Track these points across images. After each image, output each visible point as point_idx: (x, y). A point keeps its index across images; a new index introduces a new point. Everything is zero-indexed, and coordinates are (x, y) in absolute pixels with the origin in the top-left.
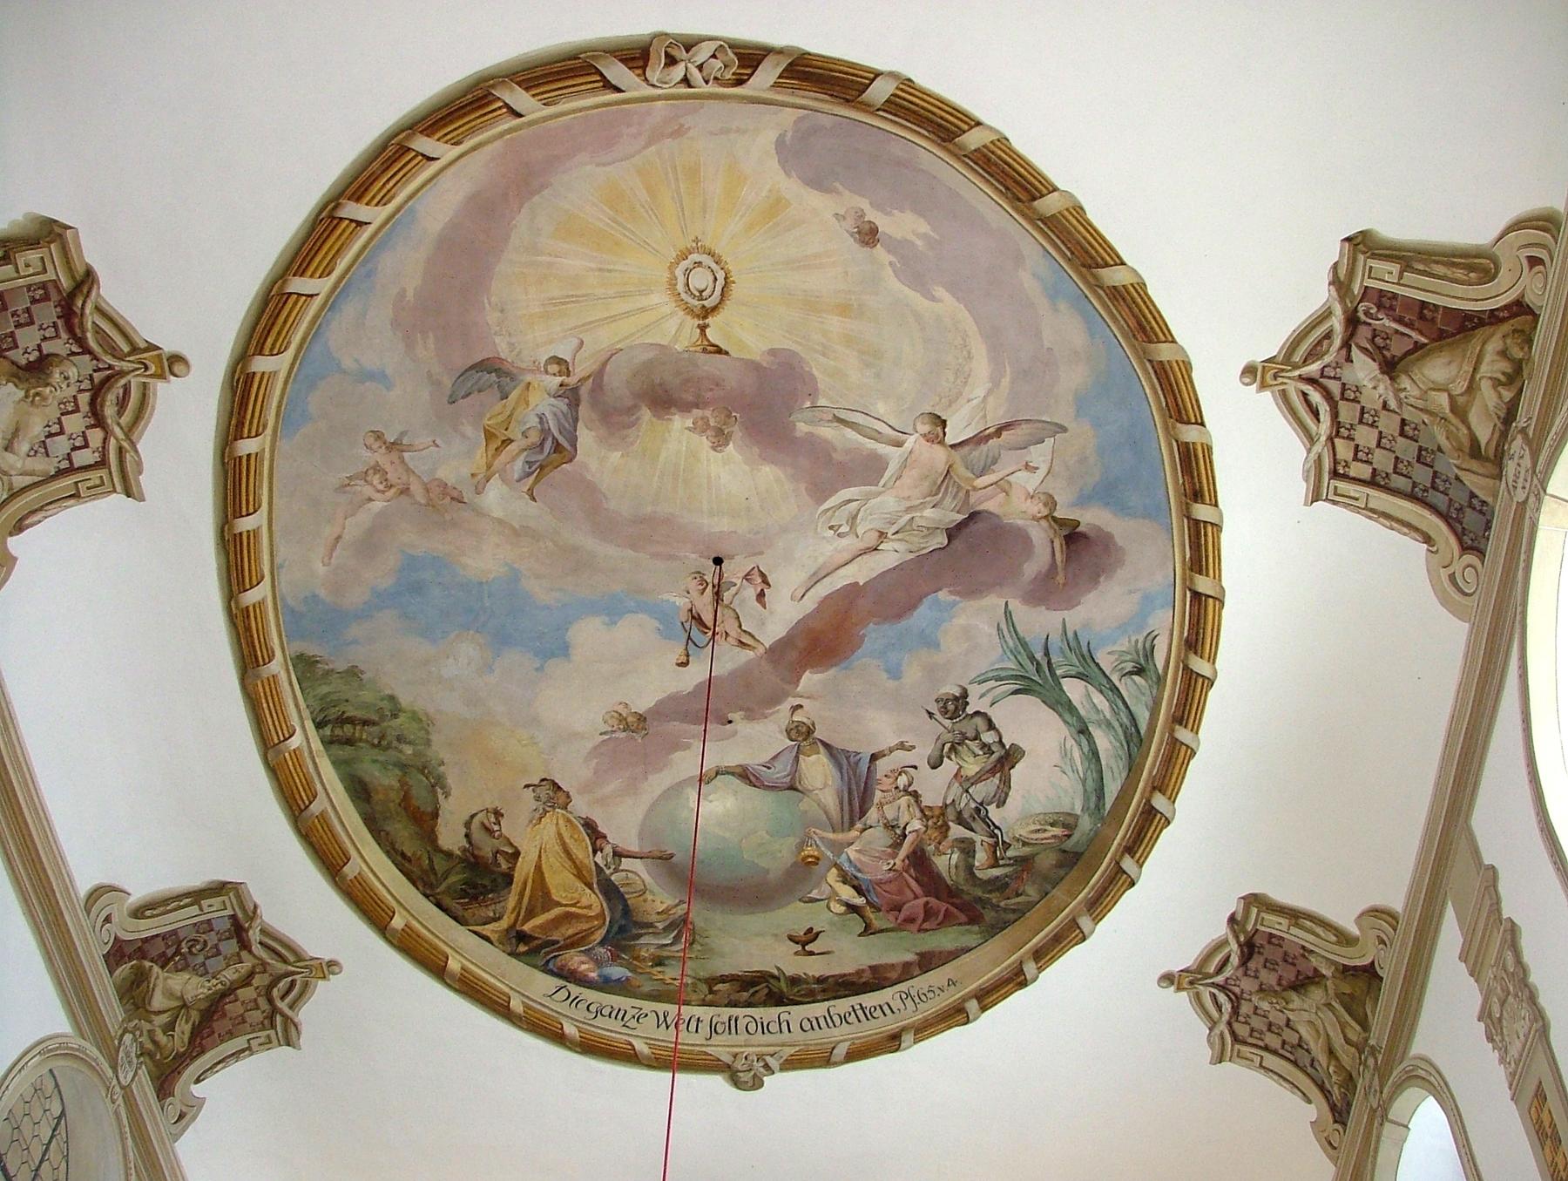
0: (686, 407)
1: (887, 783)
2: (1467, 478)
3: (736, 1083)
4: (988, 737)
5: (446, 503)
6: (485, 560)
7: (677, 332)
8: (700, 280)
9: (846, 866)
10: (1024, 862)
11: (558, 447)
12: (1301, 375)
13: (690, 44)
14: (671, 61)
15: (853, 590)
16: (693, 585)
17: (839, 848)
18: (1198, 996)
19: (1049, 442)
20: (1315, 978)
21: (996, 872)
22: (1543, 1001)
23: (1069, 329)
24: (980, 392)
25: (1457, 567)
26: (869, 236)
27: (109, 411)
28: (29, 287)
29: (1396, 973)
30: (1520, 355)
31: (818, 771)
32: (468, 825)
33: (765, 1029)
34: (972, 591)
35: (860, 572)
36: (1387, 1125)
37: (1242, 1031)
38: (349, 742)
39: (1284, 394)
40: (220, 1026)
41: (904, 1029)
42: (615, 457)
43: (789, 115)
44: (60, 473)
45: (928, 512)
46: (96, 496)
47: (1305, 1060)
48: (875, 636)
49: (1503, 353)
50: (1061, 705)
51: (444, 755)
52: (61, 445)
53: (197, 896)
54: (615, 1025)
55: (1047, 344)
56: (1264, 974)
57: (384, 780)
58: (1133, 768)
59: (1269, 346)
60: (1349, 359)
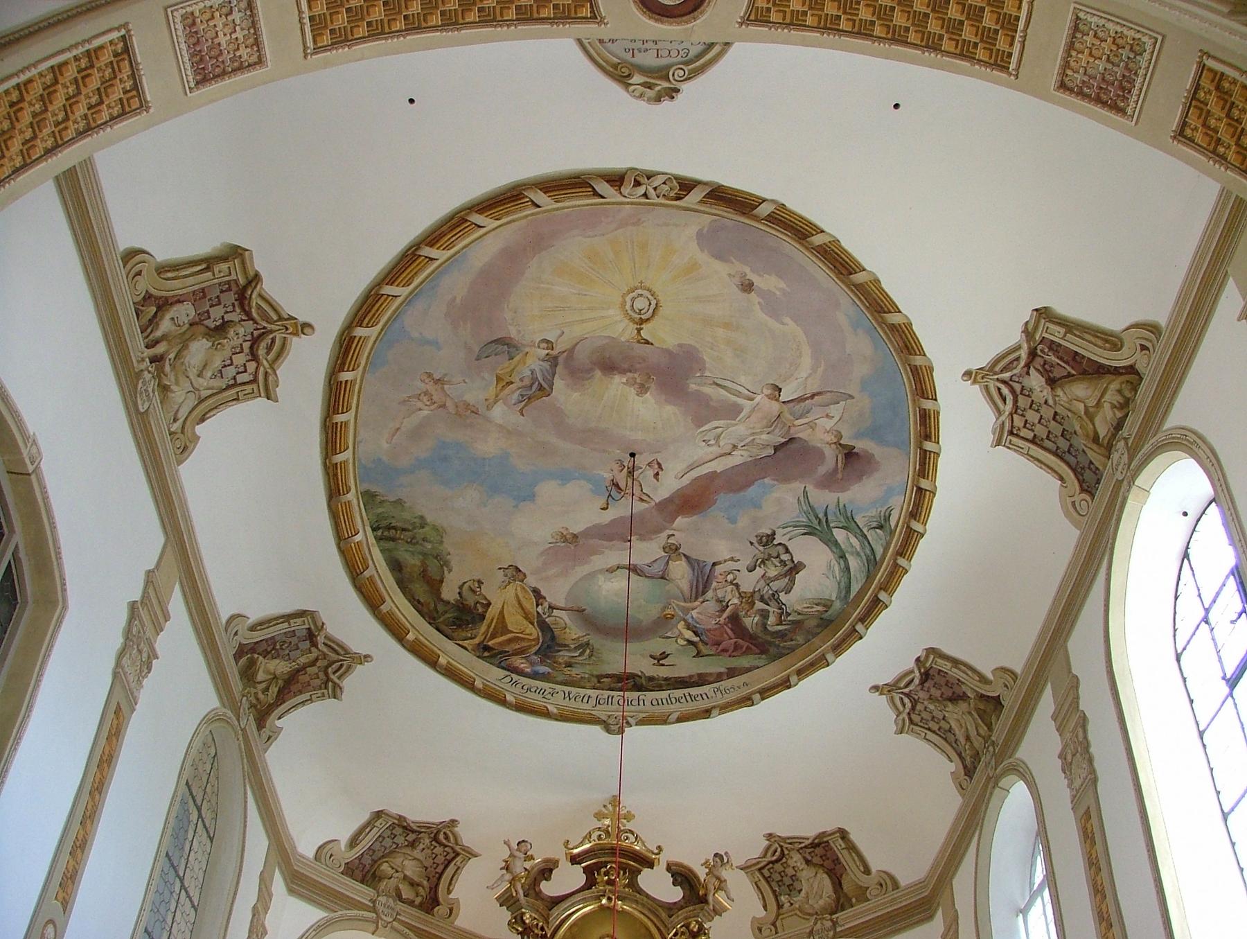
0: (623, 372)
1: (721, 578)
2: (1090, 453)
3: (608, 731)
4: (785, 557)
5: (468, 413)
6: (489, 446)
7: (623, 331)
8: (640, 304)
9: (690, 621)
10: (797, 624)
11: (541, 388)
12: (999, 379)
13: (650, 176)
14: (637, 184)
15: (713, 476)
16: (616, 467)
17: (687, 611)
18: (892, 699)
19: (842, 403)
20: (963, 697)
21: (780, 628)
22: (1095, 765)
23: (863, 348)
24: (805, 375)
25: (1077, 498)
26: (748, 287)
27: (261, 352)
28: (220, 284)
29: (1012, 707)
30: (1129, 395)
31: (680, 570)
32: (461, 587)
33: (630, 703)
34: (786, 480)
35: (718, 466)
36: (997, 790)
37: (916, 718)
38: (393, 539)
39: (987, 387)
40: (294, 688)
41: (714, 707)
42: (576, 395)
43: (708, 218)
44: (229, 387)
45: (764, 436)
46: (248, 399)
47: (952, 738)
48: (723, 500)
49: (1119, 391)
50: (832, 543)
51: (450, 550)
52: (231, 371)
53: (288, 617)
54: (539, 697)
55: (848, 351)
56: (933, 691)
57: (412, 561)
58: (870, 577)
59: (981, 360)
60: (1028, 373)
